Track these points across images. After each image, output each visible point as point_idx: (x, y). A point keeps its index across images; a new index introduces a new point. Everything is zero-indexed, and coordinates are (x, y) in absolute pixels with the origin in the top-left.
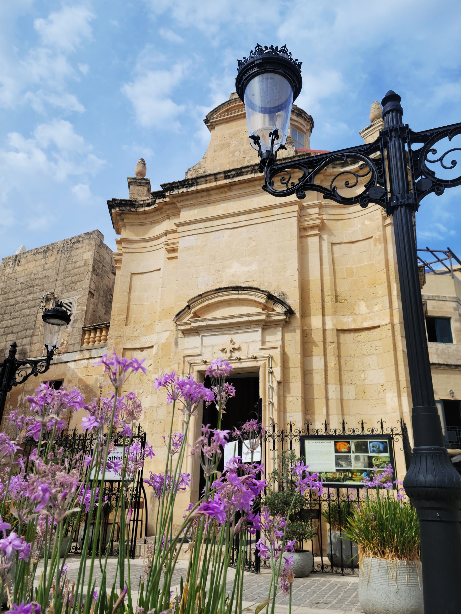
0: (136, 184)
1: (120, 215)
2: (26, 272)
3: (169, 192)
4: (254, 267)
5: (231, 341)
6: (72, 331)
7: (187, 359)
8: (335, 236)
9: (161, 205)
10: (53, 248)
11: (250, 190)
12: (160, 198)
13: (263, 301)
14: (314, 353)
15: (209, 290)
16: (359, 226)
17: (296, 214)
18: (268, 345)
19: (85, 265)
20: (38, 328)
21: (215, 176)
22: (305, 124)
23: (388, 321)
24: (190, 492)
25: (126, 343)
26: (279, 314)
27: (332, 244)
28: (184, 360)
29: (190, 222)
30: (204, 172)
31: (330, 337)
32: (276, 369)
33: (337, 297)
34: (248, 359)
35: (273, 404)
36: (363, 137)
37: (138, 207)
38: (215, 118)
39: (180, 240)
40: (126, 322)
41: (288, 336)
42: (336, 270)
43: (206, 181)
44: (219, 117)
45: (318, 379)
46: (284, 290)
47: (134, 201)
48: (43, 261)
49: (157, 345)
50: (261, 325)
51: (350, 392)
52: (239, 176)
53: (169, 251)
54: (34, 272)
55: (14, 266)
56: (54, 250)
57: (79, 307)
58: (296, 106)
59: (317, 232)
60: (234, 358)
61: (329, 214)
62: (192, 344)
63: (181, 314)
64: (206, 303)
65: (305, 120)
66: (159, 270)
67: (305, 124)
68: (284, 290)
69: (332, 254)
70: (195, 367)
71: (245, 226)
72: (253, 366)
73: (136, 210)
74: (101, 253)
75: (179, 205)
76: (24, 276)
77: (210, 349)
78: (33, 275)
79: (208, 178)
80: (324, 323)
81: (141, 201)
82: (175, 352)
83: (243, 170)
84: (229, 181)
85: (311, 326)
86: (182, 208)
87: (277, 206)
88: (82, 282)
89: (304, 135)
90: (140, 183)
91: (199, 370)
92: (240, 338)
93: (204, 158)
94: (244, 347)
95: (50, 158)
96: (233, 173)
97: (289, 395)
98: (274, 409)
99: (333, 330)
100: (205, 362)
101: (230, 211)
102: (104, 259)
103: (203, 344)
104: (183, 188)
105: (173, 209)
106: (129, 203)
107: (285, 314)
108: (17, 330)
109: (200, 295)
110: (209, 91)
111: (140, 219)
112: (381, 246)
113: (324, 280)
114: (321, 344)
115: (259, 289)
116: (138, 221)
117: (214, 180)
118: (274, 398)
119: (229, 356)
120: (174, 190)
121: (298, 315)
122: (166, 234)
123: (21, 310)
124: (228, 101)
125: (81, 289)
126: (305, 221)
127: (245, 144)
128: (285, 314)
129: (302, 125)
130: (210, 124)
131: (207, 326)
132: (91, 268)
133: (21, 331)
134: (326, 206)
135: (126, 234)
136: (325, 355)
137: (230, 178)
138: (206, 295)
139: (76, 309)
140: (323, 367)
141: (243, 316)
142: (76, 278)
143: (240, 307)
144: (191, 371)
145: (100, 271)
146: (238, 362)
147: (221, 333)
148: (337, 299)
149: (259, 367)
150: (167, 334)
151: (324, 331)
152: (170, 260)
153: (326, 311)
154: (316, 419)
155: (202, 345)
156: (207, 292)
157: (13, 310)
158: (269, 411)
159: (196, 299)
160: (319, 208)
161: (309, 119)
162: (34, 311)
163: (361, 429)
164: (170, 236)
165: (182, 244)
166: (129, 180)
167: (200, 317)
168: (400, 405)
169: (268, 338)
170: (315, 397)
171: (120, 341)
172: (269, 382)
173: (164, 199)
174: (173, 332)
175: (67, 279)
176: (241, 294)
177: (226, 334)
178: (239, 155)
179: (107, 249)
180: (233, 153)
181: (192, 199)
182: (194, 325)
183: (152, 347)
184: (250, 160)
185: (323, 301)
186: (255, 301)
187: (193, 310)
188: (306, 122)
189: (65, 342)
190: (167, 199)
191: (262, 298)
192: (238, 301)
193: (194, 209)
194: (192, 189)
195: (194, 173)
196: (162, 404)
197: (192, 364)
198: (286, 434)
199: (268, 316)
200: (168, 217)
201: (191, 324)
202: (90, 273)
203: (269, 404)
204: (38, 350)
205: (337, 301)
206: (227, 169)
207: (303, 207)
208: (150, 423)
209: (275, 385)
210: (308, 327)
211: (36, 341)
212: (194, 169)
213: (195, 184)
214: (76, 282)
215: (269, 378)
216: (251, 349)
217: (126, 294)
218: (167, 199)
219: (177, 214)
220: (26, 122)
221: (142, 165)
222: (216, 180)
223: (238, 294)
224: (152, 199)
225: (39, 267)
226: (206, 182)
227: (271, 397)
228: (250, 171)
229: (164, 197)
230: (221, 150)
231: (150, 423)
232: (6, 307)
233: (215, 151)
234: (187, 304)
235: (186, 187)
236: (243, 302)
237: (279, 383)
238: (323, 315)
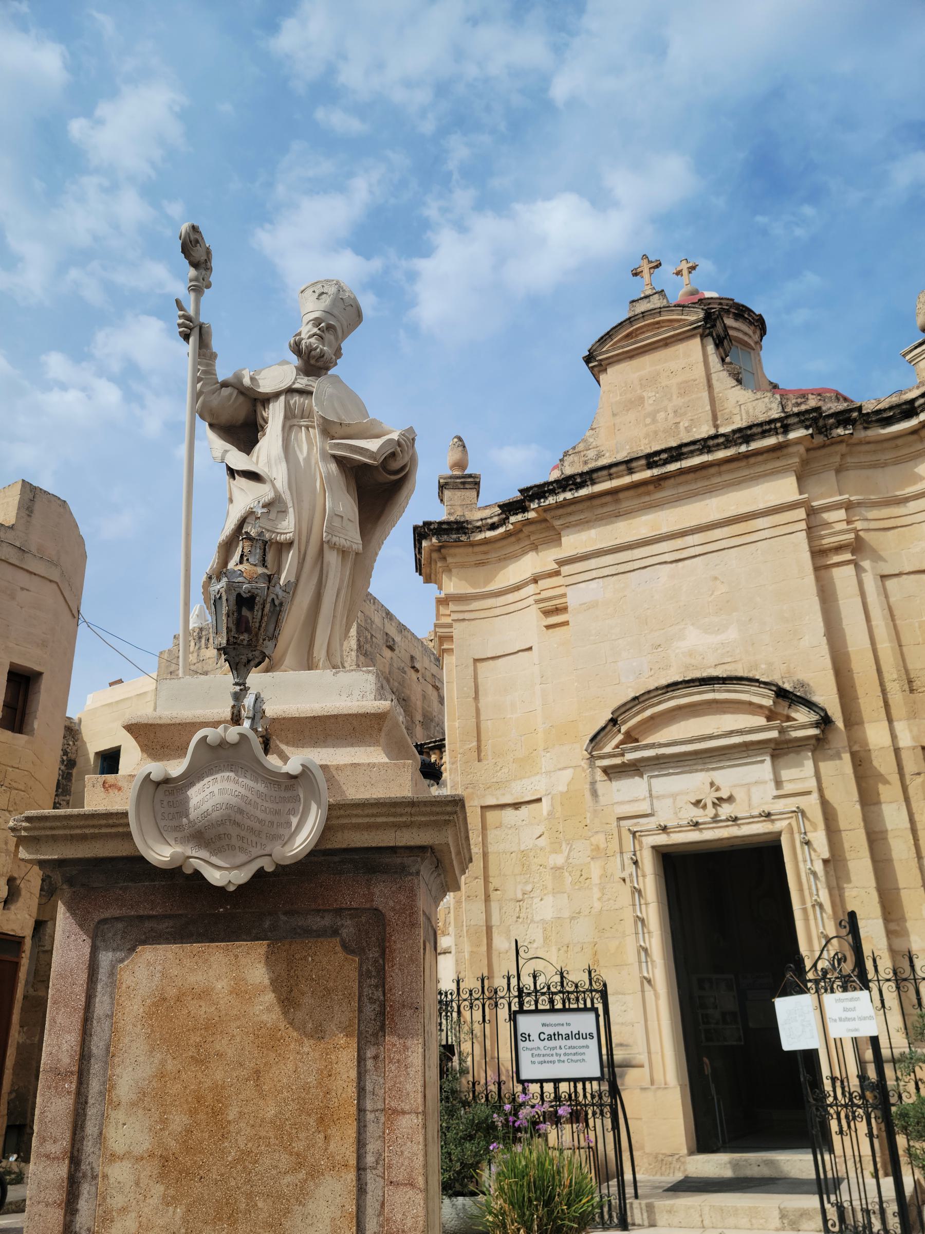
0: (456, 487)
1: (439, 549)
3: (536, 501)
4: (732, 634)
5: (712, 784)
7: (623, 823)
8: (885, 561)
9: (519, 526)
11: (700, 484)
12: (517, 514)
13: (768, 702)
14: (883, 798)
15: (652, 688)
17: (803, 525)
18: (788, 788)
21: (628, 465)
22: (751, 333)
24: (679, 1088)
25: (484, 796)
26: (803, 727)
27: (883, 577)
28: (619, 826)
29: (586, 556)
30: (599, 456)
32: (814, 834)
33: (910, 682)
34: (753, 817)
35: (821, 906)
36: (910, 362)
37: (472, 532)
38: (607, 352)
39: (569, 591)
40: (479, 755)
41: (827, 767)
42: (899, 628)
43: (610, 475)
44: (614, 349)
46: (803, 675)
47: (463, 522)
49: (550, 796)
50: (770, 750)
52: (677, 461)
53: (547, 613)
55: (199, 649)
58: (733, 300)
59: (848, 556)
60: (723, 818)
61: (867, 520)
62: (629, 793)
63: (599, 737)
64: (648, 713)
65: (751, 323)
66: (530, 649)
67: (751, 333)
69: (887, 597)
70: (644, 839)
71: (700, 555)
72: (767, 831)
73: (469, 538)
74: (367, 613)
75: (556, 523)
77: (669, 801)
79: (613, 470)
80: (894, 737)
81: (478, 521)
82: (595, 811)
83: (685, 450)
84: (656, 472)
85: (867, 744)
86: (562, 529)
87: (761, 513)
89: (752, 352)
90: (463, 483)
91: (655, 844)
92: (729, 778)
93: (592, 429)
94: (739, 795)
95: (130, 396)
96: (664, 456)
97: (850, 886)
98: (824, 915)
99: (914, 748)
100: (664, 829)
101: (665, 529)
102: (372, 622)
103: (654, 793)
104: (564, 491)
105: (547, 532)
106: (455, 526)
107: (817, 725)
109: (635, 698)
110: (426, 225)
111: (476, 553)
113: (879, 650)
114: (895, 778)
115: (757, 681)
116: (473, 559)
117: (625, 472)
118: (821, 893)
119: (712, 815)
120: (546, 498)
121: (840, 724)
122: (535, 580)
124: (630, 318)
126: (822, 537)
127: (675, 397)
128: (817, 725)
129: (746, 334)
130: (596, 363)
131: (657, 757)
134: (859, 503)
135: (452, 585)
136: (907, 800)
137: (657, 466)
138: (646, 697)
140: (908, 825)
141: (731, 733)
143: (718, 716)
144: (637, 848)
145: (367, 646)
146: (732, 825)
147: (687, 768)
148: (911, 685)
149: (779, 834)
151: (897, 751)
152: (551, 631)
153: (894, 712)
154: (910, 930)
155: (651, 795)
156: (649, 692)
158: (816, 919)
159: (628, 707)
160: (846, 510)
161: (757, 321)
164: (543, 584)
165: (574, 597)
166: (442, 481)
167: (637, 740)
169: (785, 774)
170: (901, 885)
171: (473, 793)
172: (805, 861)
173: (526, 514)
174: (584, 771)
176: (719, 691)
177: (697, 771)
178: (666, 419)
179: (374, 603)
180: (653, 415)
181: (582, 511)
182: (630, 756)
183: (539, 800)
184: (690, 426)
185: (884, 691)
186: (750, 703)
187: (624, 729)
188: (752, 328)
190: (531, 515)
191: (764, 696)
192: (714, 705)
193: (589, 529)
194: (583, 492)
195: (576, 459)
196: (579, 913)
197: (637, 834)
198: (904, 976)
199: (782, 731)
200: (535, 547)
201: (623, 755)
202: (354, 654)
203: (813, 906)
205: (912, 691)
206: (648, 451)
207: (813, 510)
208: (559, 950)
209: (819, 867)
210: (860, 747)
212: (575, 451)
213: (589, 483)
215: (803, 853)
216: (752, 799)
217: (471, 700)
218: (531, 515)
219: (555, 539)
220: (73, 327)
221: (460, 449)
222: (631, 471)
223: (714, 691)
224: (499, 515)
226: (611, 477)
227: (815, 892)
228: (698, 449)
229: (525, 510)
230: (628, 410)
231: (559, 950)
233: (614, 415)
234: (611, 716)
235: (570, 490)
236: (724, 705)
237: (825, 862)
238: (890, 720)
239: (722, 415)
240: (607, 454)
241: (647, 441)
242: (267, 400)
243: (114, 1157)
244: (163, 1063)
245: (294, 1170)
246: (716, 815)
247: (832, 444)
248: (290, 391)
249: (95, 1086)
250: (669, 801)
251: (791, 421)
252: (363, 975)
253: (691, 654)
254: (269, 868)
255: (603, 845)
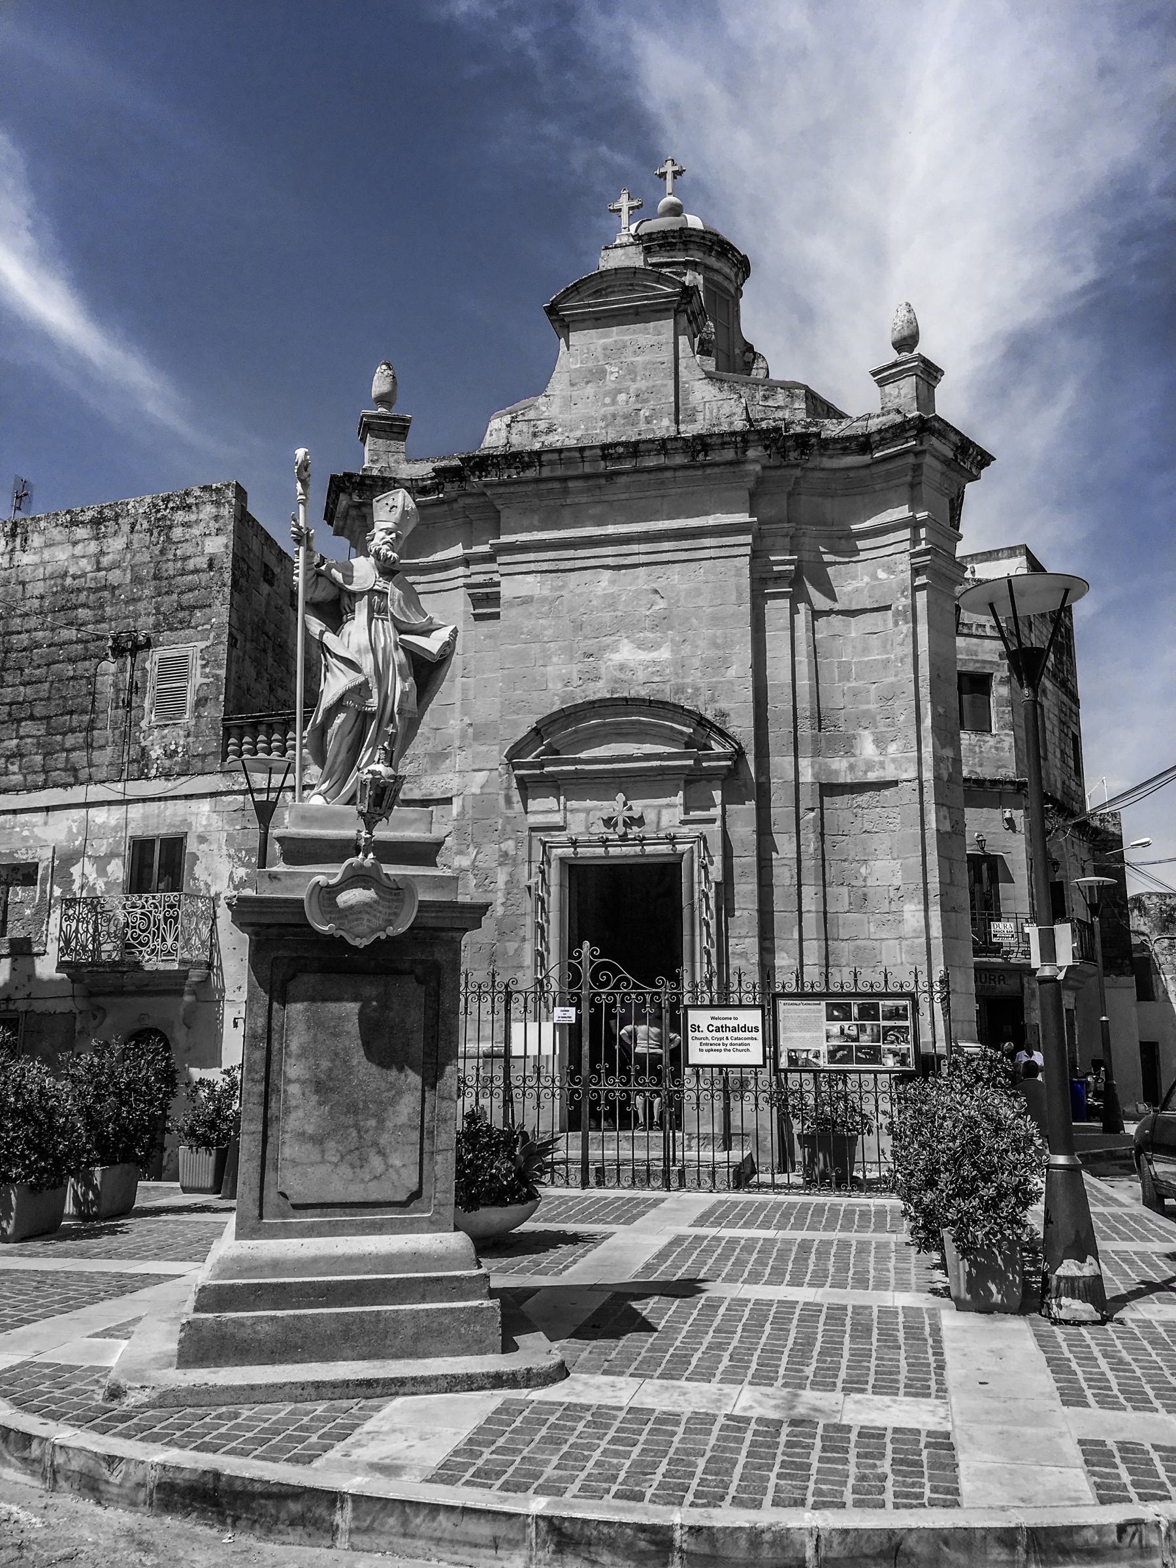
2: (49, 569)
4: (664, 654)
6: (196, 725)
10: (117, 516)
16: (866, 579)
17: (748, 550)
19: (211, 566)
20: (102, 712)
23: (912, 773)
28: (530, 836)
31: (808, 799)
39: (504, 581)
45: (783, 876)
48: (93, 547)
51: (840, 898)
54: (71, 571)
56: (120, 520)
57: (207, 670)
68: (723, 705)
76: (44, 579)
78: (69, 581)
88: (207, 610)
99: (813, 784)
100: (574, 843)
102: (250, 550)
108: (44, 713)
112: (906, 628)
123: (48, 665)
125: (208, 627)
132: (227, 577)
133: (56, 715)
139: (198, 674)
142: (188, 598)
148: (819, 719)
150: (481, 777)
157: (26, 662)
161: (741, 262)
162: (86, 670)
163: (883, 984)
165: (509, 589)
168: (927, 926)
175: (166, 598)
189: (180, 749)
194: (530, 473)
199: (698, 761)
202: (227, 590)
204: (111, 764)
211: (102, 742)
214: (192, 608)
225: (85, 561)
230: (587, 383)
232: (6, 653)
239: (686, 410)
240: (560, 430)
241: (603, 424)
242: (355, 596)
243: (289, 1081)
244: (316, 1035)
245: (388, 1090)
246: (626, 834)
247: (787, 466)
248: (372, 592)
249: (276, 1045)
250: (583, 815)
251: (751, 437)
252: (427, 995)
253: (622, 667)
254: (383, 937)
255: (512, 852)
